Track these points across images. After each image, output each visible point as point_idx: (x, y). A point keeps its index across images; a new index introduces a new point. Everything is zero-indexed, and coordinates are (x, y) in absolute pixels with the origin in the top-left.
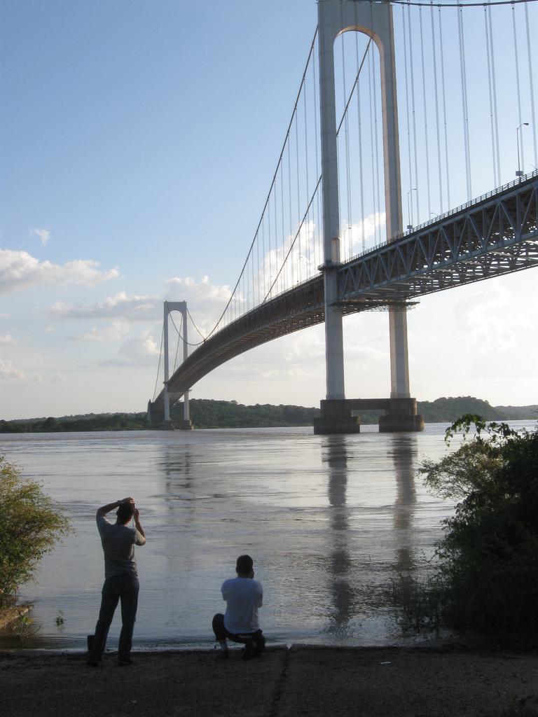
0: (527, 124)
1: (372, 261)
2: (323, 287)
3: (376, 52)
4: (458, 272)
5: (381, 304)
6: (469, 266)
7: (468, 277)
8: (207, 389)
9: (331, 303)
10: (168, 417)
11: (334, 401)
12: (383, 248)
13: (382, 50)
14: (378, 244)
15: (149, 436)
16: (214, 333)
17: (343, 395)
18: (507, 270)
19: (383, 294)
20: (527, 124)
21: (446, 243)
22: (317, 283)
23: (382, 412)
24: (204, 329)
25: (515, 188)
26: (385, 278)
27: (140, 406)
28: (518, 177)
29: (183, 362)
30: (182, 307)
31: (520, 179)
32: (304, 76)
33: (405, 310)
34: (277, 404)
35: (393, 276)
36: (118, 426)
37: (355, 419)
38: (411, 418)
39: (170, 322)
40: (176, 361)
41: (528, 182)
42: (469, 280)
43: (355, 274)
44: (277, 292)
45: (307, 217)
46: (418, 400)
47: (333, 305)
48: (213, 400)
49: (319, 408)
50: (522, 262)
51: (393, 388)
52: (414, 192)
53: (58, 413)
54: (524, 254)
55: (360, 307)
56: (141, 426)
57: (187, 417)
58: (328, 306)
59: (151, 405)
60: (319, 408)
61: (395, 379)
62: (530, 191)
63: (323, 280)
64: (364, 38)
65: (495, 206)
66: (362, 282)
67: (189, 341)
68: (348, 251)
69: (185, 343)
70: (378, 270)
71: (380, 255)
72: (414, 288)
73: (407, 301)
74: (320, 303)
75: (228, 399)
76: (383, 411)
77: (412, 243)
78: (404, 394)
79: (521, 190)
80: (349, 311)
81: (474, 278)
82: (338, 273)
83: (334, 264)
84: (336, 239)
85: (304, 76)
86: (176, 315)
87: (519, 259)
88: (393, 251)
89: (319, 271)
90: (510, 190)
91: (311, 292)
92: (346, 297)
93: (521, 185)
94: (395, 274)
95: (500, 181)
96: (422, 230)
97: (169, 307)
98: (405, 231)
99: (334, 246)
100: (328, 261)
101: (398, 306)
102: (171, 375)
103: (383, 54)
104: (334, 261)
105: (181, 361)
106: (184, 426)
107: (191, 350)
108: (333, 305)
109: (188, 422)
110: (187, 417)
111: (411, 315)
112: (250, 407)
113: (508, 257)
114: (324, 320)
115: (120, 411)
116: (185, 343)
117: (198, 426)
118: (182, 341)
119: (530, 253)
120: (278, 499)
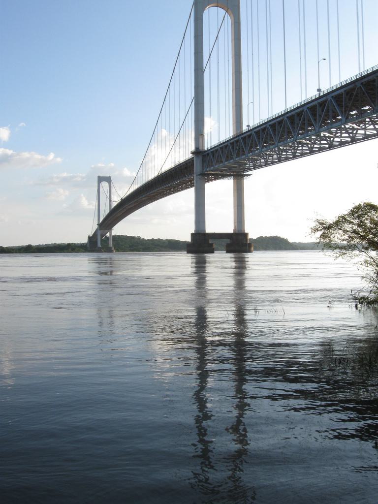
0: (325, 59)
1: (261, 132)
2: (193, 165)
3: (229, 21)
4: (277, 154)
5: (230, 175)
6: (270, 155)
7: (283, 158)
8: (121, 229)
9: (198, 174)
10: (99, 245)
11: (199, 233)
12: (231, 139)
13: (233, 18)
14: (270, 116)
15: (7, 278)
16: (127, 194)
17: (205, 230)
18: (276, 162)
19: (230, 169)
20: (325, 59)
21: (289, 129)
22: (190, 162)
23: (228, 241)
24: (121, 192)
25: (316, 99)
26: (232, 158)
27: (82, 239)
28: (318, 92)
29: (108, 212)
30: (108, 179)
31: (320, 93)
32: (184, 35)
33: (243, 179)
34: (164, 238)
35: (226, 161)
36: (70, 250)
37: (212, 245)
38: (246, 245)
39: (101, 189)
40: (105, 211)
41: (325, 95)
42: (284, 160)
43: (213, 156)
44: (167, 167)
45: (184, 124)
46: (346, 213)
47: (199, 175)
48: (126, 236)
49: (190, 241)
50: (300, 153)
51: (235, 227)
52: (251, 105)
53: (35, 243)
54: (300, 148)
55: (217, 177)
56: (83, 250)
57: (111, 244)
58: (197, 176)
59: (90, 238)
60: (190, 241)
61: (236, 221)
62: (326, 101)
63: (194, 160)
64: (222, 12)
65: (303, 111)
66: (217, 161)
67: (112, 200)
68: (211, 141)
69: (110, 201)
70: (228, 153)
71: (229, 144)
72: (249, 165)
73: (245, 173)
74: (191, 175)
75: (136, 235)
76: (229, 240)
77: (249, 136)
78: (242, 230)
79: (319, 101)
80: (210, 180)
81: (273, 163)
82: (203, 156)
83: (201, 150)
84: (202, 135)
85: (184, 35)
86: (105, 184)
87: (298, 152)
88: (237, 141)
89: (191, 155)
90: (313, 101)
91: (186, 168)
92: (208, 170)
93: (320, 97)
94: (238, 156)
95: (211, 142)
96: (256, 128)
97: (101, 179)
98: (245, 128)
99: (201, 140)
100: (197, 148)
101: (239, 176)
102: (101, 220)
103: (233, 22)
104: (201, 148)
105: (107, 212)
106: (109, 250)
107: (114, 204)
108: (199, 175)
109: (111, 248)
110: (111, 244)
111: (247, 182)
112: (148, 240)
113: (307, 144)
114: (193, 186)
115: (71, 242)
116: (110, 201)
117: (118, 250)
118: (108, 200)
119: (304, 148)
120: (222, 290)
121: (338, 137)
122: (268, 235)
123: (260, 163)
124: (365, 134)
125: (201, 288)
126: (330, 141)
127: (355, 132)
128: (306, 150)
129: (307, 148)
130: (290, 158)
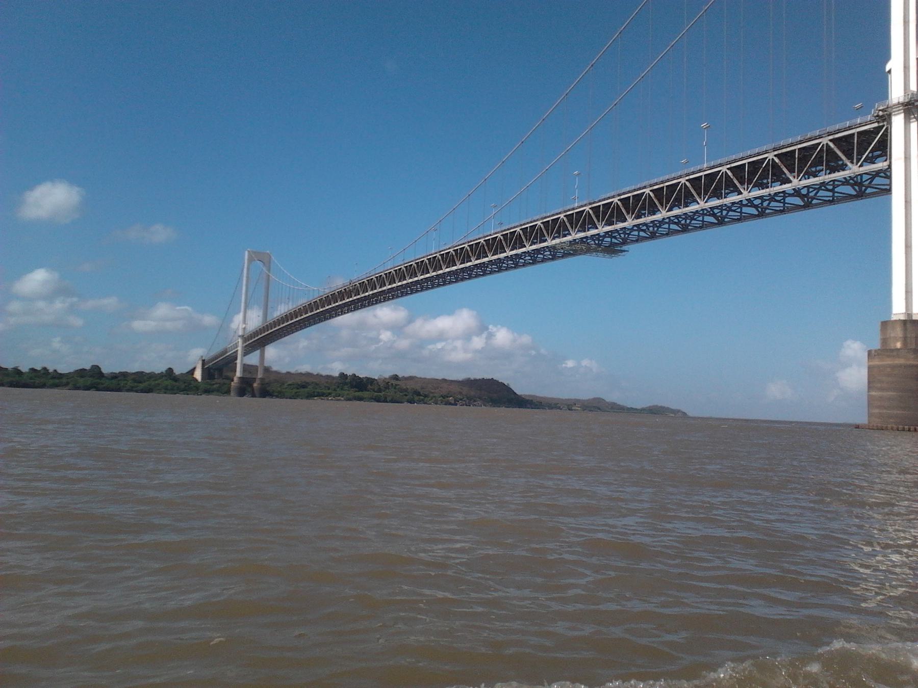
50: (489, 271)
121: (522, 259)
122: (479, 377)
123: (407, 291)
124: (638, 235)
125: (906, 105)
126: (484, 270)
127: (536, 256)
128: (495, 268)
129: (496, 267)
130: (466, 279)
